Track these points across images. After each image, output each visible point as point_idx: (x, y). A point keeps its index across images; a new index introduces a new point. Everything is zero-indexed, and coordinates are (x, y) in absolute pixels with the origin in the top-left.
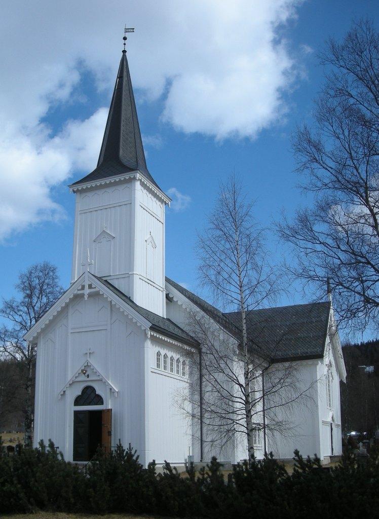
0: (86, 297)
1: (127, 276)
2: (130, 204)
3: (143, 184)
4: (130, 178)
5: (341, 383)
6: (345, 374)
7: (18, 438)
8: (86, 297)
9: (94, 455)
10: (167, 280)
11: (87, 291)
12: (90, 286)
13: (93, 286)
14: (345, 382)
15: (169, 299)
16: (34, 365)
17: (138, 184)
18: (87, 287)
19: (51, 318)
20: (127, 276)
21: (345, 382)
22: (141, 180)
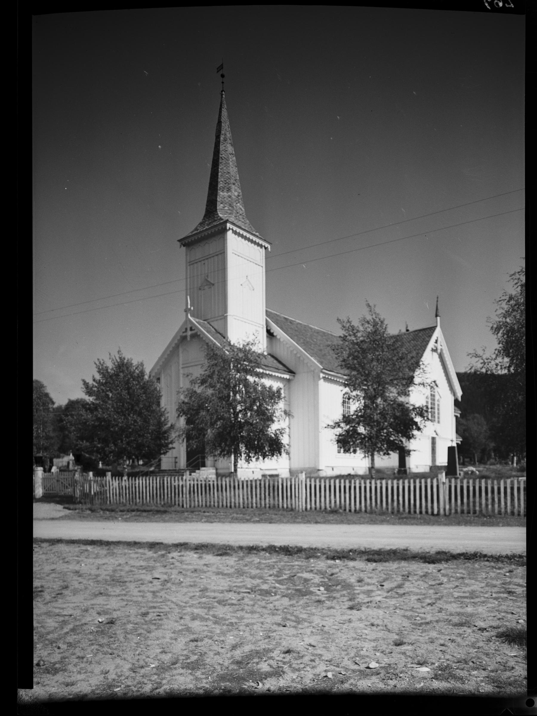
0: (189, 338)
1: (222, 317)
2: (222, 254)
3: (235, 233)
4: (222, 228)
5: (456, 403)
6: (459, 393)
7: (116, 674)
8: (189, 338)
9: (87, 441)
10: (268, 314)
11: (189, 333)
12: (191, 329)
13: (193, 328)
14: (460, 399)
15: (270, 334)
16: (434, 331)
17: (230, 234)
18: (189, 329)
19: (257, 242)
20: (222, 317)
21: (460, 399)
22: (232, 229)
